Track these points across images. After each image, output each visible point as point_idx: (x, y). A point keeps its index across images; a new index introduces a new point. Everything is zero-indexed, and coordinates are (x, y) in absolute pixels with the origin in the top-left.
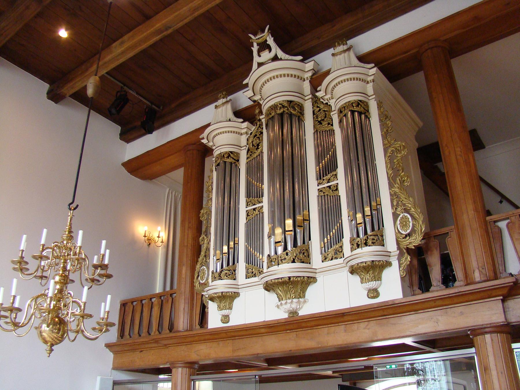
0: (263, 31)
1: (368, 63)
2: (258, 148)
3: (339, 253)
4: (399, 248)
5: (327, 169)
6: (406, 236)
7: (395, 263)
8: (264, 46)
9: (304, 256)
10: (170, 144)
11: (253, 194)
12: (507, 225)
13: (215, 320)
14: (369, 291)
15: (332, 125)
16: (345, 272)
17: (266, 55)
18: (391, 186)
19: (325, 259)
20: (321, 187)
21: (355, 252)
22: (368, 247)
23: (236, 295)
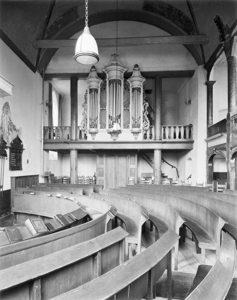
1: (144, 77)
2: (104, 90)
3: (128, 127)
4: (143, 129)
6: (146, 127)
7: (142, 133)
9: (96, 126)
10: (71, 74)
13: (90, 138)
15: (129, 91)
19: (124, 128)
20: (124, 108)
21: (91, 129)
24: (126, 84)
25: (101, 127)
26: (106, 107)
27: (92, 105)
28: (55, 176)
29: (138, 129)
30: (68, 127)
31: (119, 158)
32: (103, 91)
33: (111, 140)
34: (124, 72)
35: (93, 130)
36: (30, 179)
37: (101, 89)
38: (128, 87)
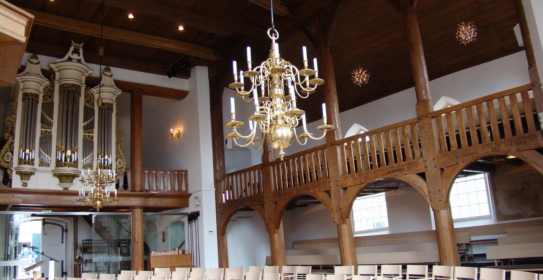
0: (80, 44)
1: (120, 89)
5: (89, 128)
8: (76, 51)
11: (46, 123)
13: (17, 182)
14: (26, 186)
16: (52, 175)
17: (75, 56)
18: (116, 146)
23: (32, 174)
26: (51, 129)
29: (31, 166)
33: (60, 188)
34: (87, 74)
35: (27, 168)
36: (164, 266)
37: (44, 96)
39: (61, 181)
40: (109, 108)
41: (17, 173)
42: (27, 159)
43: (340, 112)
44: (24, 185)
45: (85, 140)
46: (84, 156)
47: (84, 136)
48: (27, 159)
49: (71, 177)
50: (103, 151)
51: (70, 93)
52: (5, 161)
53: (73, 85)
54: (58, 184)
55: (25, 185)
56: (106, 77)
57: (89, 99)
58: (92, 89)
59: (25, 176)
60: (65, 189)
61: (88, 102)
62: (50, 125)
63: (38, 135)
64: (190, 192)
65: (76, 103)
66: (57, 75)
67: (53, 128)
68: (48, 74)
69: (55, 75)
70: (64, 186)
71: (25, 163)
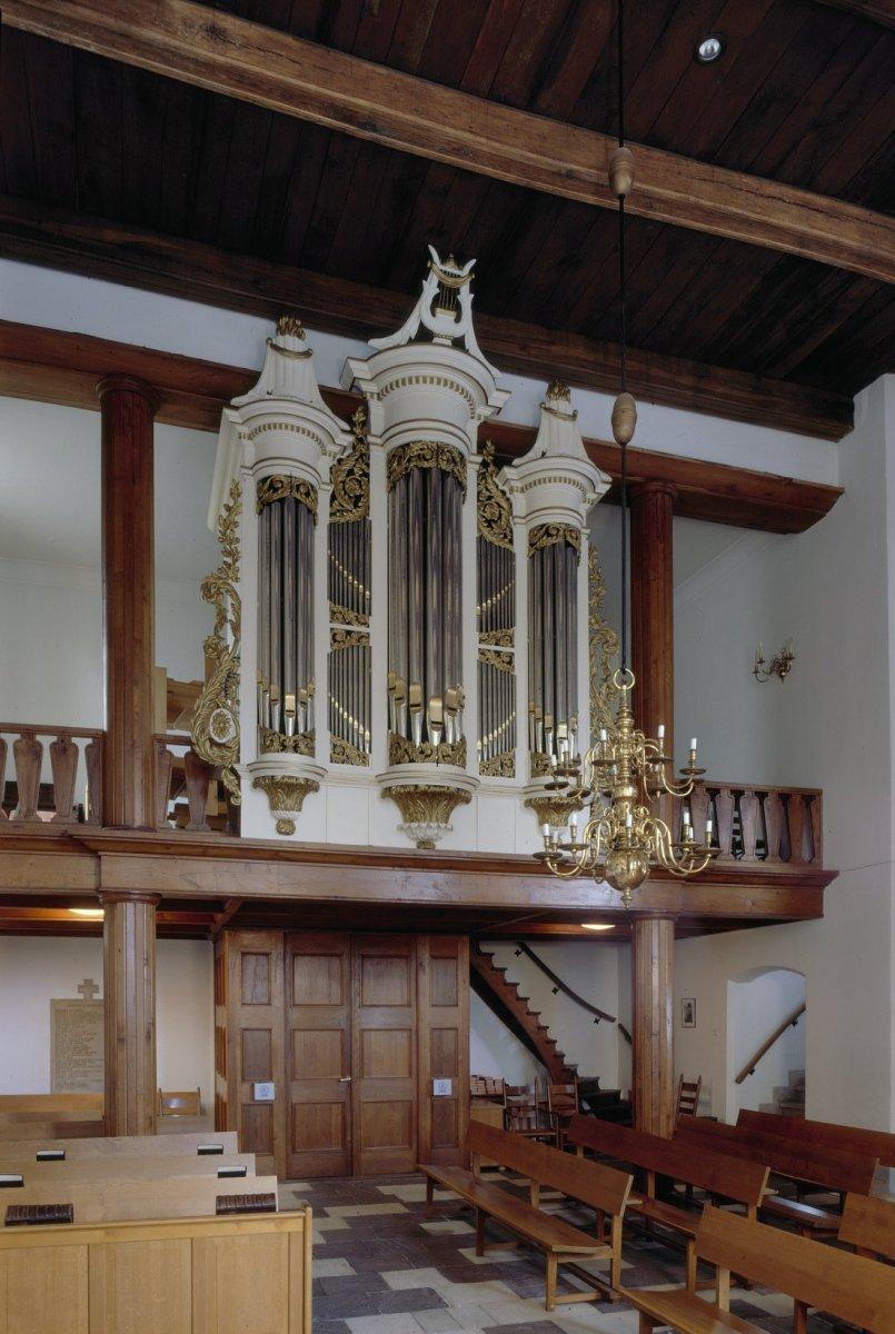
5: (496, 622)
8: (447, 299)
11: (351, 601)
12: (53, 746)
13: (257, 821)
16: (376, 792)
17: (443, 323)
18: (593, 697)
22: (296, 755)
23: (309, 787)
24: (490, 498)
25: (339, 755)
26: (366, 624)
27: (282, 603)
28: (567, 1061)
30: (82, 733)
31: (369, 967)
32: (347, 511)
33: (404, 843)
35: (290, 765)
37: (333, 498)
38: (500, 518)
39: (409, 816)
40: (568, 544)
41: (256, 784)
42: (290, 731)
43: (676, 938)
44: (285, 828)
45: (484, 668)
46: (484, 730)
47: (482, 653)
48: (290, 731)
49: (444, 800)
50: (549, 709)
51: (426, 483)
52: (212, 741)
53: (439, 450)
54: (401, 828)
55: (286, 827)
56: (555, 421)
57: (495, 517)
58: (506, 470)
59: (285, 791)
60: (424, 843)
61: (489, 523)
62: (362, 608)
63: (322, 647)
64: (827, 865)
65: (450, 523)
66: (377, 410)
67: (372, 621)
68: (346, 403)
69: (366, 412)
70: (421, 835)
71: (284, 748)
